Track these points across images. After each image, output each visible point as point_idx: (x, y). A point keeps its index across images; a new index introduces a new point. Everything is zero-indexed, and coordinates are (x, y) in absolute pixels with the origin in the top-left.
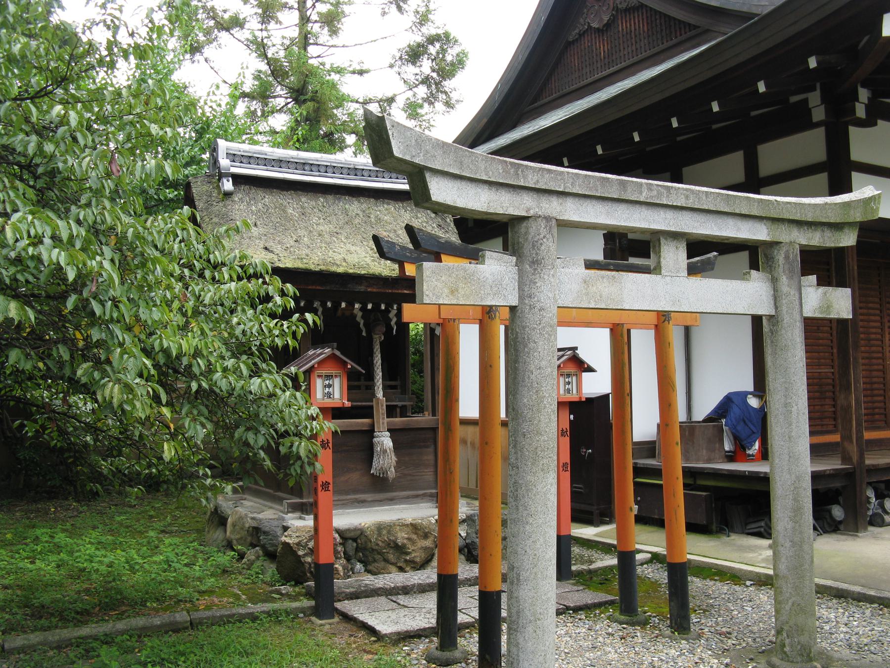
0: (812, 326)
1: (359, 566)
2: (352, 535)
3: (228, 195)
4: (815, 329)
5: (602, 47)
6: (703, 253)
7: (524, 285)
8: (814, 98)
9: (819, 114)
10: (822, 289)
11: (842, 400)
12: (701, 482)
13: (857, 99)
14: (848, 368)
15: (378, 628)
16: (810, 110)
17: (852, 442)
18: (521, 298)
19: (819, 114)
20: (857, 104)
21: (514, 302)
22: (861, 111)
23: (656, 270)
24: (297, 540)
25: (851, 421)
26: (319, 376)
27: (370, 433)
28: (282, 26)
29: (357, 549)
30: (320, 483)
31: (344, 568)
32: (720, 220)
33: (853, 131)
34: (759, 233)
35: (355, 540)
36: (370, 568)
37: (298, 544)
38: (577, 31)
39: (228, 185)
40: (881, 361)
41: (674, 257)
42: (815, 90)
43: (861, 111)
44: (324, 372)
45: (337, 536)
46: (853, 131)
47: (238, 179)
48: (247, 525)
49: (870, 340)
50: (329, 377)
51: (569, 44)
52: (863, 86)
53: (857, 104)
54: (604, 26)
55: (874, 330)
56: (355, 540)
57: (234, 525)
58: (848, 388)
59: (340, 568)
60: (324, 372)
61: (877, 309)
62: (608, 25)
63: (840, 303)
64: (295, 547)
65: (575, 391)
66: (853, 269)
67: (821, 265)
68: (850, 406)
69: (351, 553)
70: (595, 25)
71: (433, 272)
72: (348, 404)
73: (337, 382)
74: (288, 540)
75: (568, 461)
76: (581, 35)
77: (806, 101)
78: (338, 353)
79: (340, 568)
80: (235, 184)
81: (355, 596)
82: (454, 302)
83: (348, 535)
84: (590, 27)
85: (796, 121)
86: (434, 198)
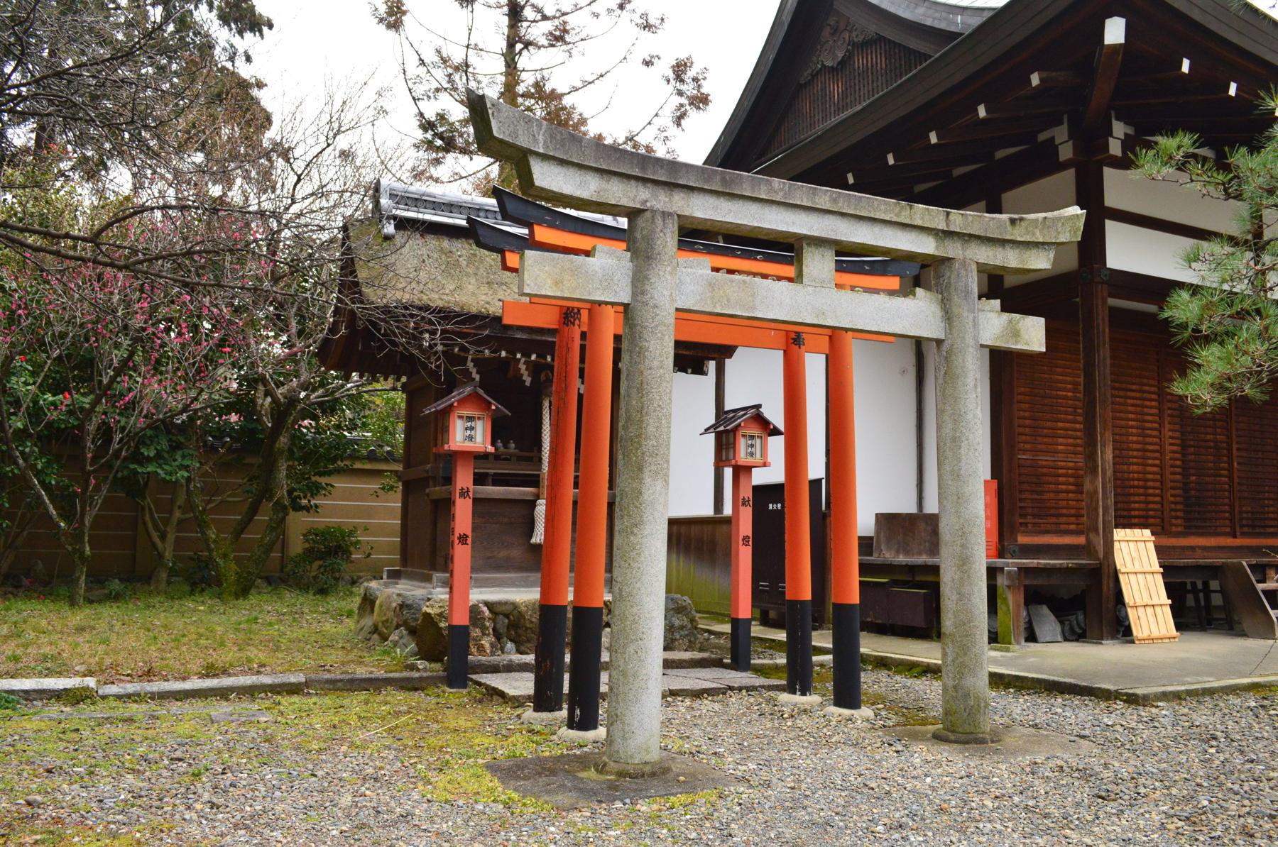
0: (1002, 363)
1: (510, 646)
2: (503, 609)
3: (388, 238)
4: (1002, 363)
5: (836, 89)
6: (854, 261)
7: (639, 281)
8: (1060, 134)
9: (1066, 152)
10: (1006, 316)
11: (1087, 486)
12: (919, 578)
13: (1109, 133)
14: (1095, 446)
15: (507, 691)
16: (1056, 147)
17: (1097, 533)
18: (634, 294)
19: (1066, 152)
20: (1111, 139)
21: (625, 298)
22: (1115, 148)
23: (798, 279)
24: (439, 611)
25: (1096, 509)
26: (460, 417)
27: (532, 504)
28: (441, 42)
29: (509, 627)
30: (457, 535)
31: (492, 645)
32: (877, 229)
33: (1107, 171)
34: (927, 246)
35: (507, 616)
36: (523, 648)
37: (441, 615)
38: (809, 71)
39: (390, 229)
40: (1157, 455)
41: (819, 265)
42: (1061, 123)
43: (1115, 148)
44: (466, 413)
45: (485, 609)
46: (1107, 171)
47: (402, 224)
48: (394, 605)
49: (1144, 429)
50: (471, 419)
51: (801, 87)
52: (1118, 119)
53: (1111, 139)
54: (839, 63)
55: (1150, 418)
56: (507, 616)
57: (381, 606)
58: (1094, 470)
59: (487, 645)
60: (466, 413)
61: (1154, 393)
62: (843, 63)
63: (1032, 334)
64: (436, 619)
65: (758, 455)
66: (1104, 331)
67: (1010, 292)
68: (1096, 492)
69: (502, 630)
70: (829, 63)
71: (536, 261)
72: (490, 449)
73: (479, 425)
74: (429, 610)
75: (750, 534)
76: (814, 76)
77: (1053, 139)
78: (481, 391)
79: (487, 645)
80: (397, 227)
81: (494, 669)
82: (559, 294)
83: (499, 609)
84: (823, 65)
85: (1038, 164)
86: (537, 183)
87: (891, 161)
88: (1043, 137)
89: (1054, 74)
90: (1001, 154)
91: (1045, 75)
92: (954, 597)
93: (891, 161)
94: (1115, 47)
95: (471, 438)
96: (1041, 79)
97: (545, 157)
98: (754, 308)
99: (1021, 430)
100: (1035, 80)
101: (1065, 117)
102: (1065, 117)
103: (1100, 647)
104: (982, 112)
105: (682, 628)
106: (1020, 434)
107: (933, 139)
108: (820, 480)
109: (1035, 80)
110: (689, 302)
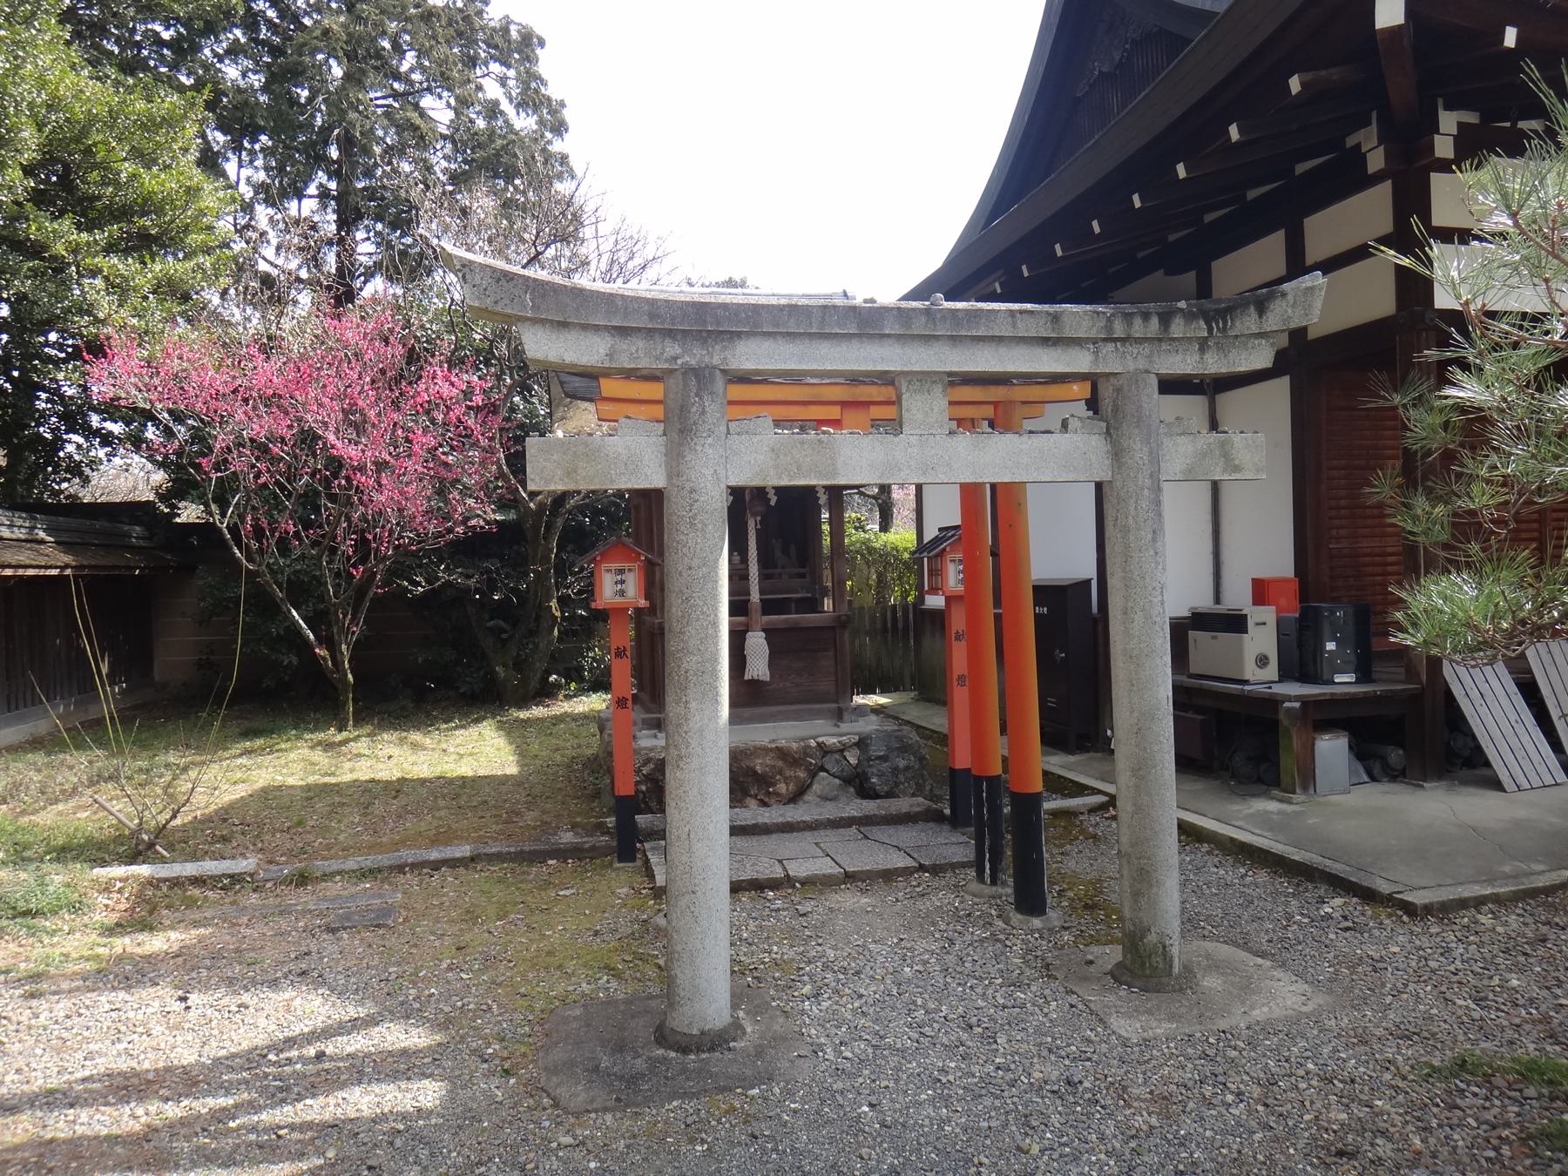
18: (670, 477)
19: (1376, 161)
22: (1444, 147)
41: (926, 410)
42: (1368, 123)
43: (1444, 147)
44: (614, 566)
50: (621, 572)
52: (1447, 108)
77: (1358, 146)
85: (1348, 178)
87: (1137, 204)
88: (1351, 141)
89: (1323, 73)
90: (1301, 168)
91: (1309, 76)
92: (1130, 809)
93: (1137, 204)
94: (1394, 32)
95: (622, 593)
96: (1302, 84)
97: (534, 321)
98: (834, 473)
99: (1333, 513)
100: (1295, 84)
101: (1374, 115)
102: (1374, 115)
103: (1420, 793)
104: (1234, 132)
105: (907, 768)
106: (1331, 518)
107: (1181, 171)
108: (1089, 581)
109: (1295, 84)
110: (743, 477)
